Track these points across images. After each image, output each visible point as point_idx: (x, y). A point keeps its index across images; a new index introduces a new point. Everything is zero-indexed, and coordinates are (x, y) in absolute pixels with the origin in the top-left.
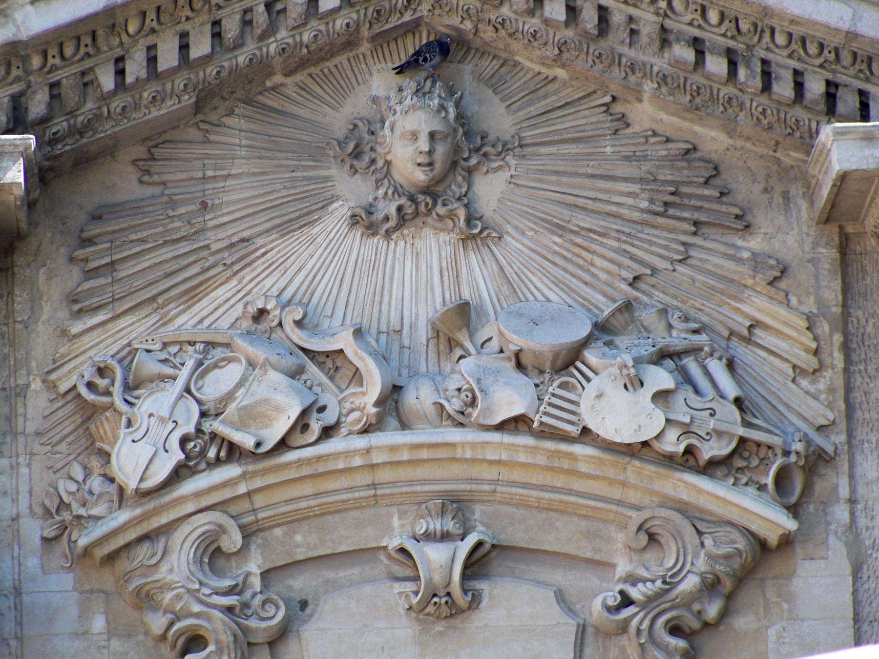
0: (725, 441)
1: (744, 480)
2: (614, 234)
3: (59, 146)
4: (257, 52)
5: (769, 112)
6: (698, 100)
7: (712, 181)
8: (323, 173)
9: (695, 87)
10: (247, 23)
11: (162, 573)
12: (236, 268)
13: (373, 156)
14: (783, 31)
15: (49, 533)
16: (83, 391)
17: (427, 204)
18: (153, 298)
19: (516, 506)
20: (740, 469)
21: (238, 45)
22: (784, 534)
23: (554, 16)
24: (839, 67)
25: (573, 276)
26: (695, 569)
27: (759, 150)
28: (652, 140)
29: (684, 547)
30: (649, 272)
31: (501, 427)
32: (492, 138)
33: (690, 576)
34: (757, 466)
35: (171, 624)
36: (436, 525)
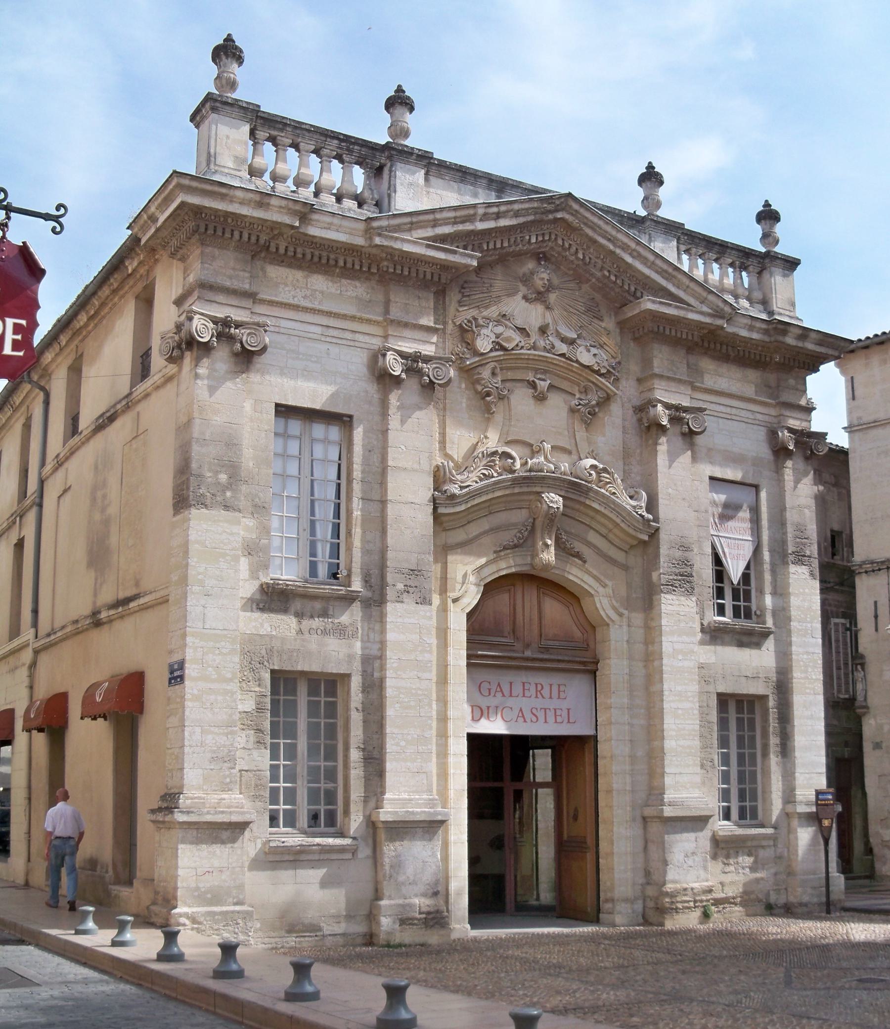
31: (560, 355)
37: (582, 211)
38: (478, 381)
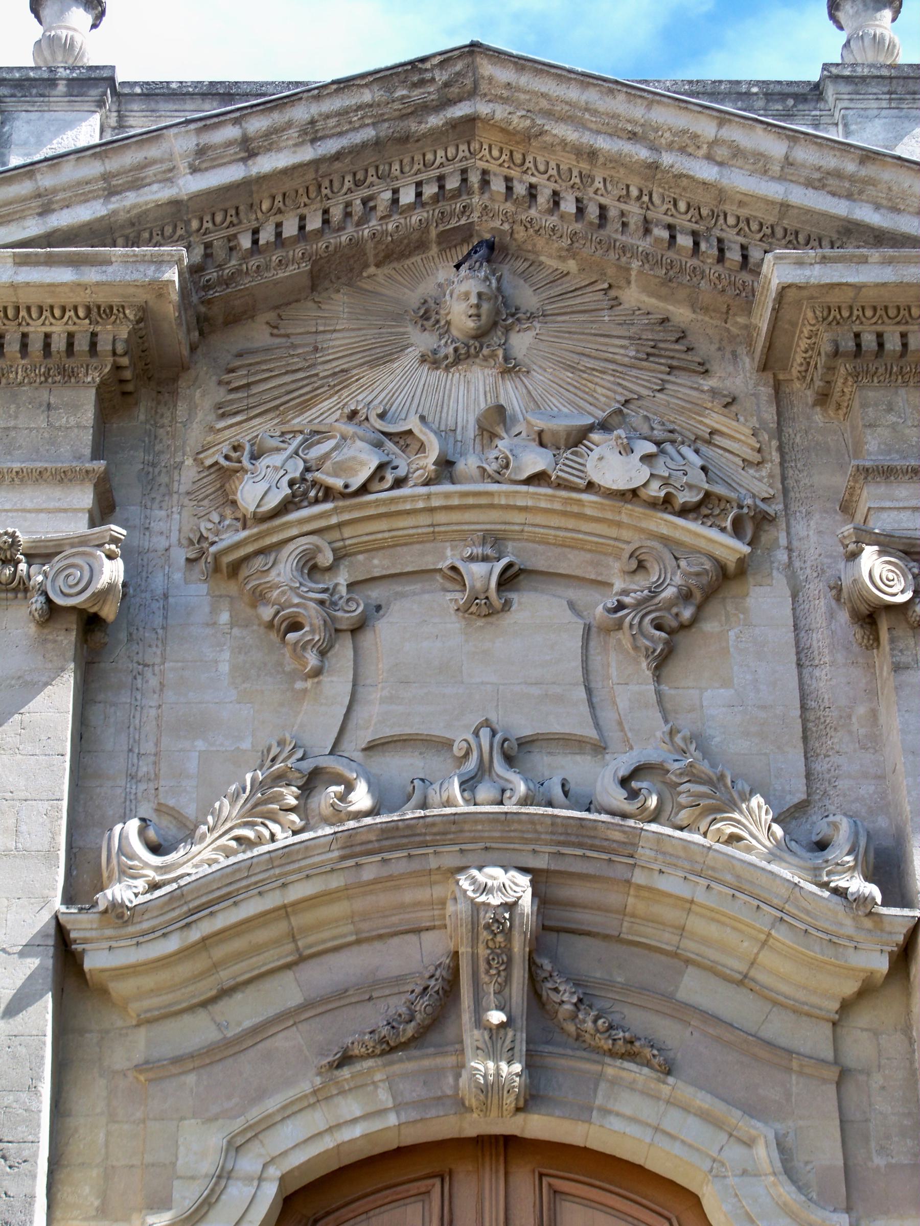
0: (694, 493)
1: (709, 523)
2: (611, 372)
3: (211, 292)
4: (355, 234)
5: (723, 276)
6: (671, 273)
7: (681, 341)
8: (402, 330)
9: (669, 261)
10: (348, 215)
11: (272, 576)
12: (337, 388)
13: (438, 317)
14: (733, 214)
15: (192, 555)
16: (222, 462)
17: (475, 348)
18: (277, 407)
19: (539, 543)
20: (706, 516)
21: (341, 228)
22: (739, 559)
23: (568, 210)
24: (774, 240)
25: (582, 399)
26: (673, 583)
27: (715, 322)
28: (637, 313)
29: (665, 568)
30: (636, 397)
31: (529, 481)
32: (523, 310)
33: (669, 587)
34: (719, 515)
35: (277, 613)
36: (478, 551)
37: (525, 80)
38: (258, 597)
